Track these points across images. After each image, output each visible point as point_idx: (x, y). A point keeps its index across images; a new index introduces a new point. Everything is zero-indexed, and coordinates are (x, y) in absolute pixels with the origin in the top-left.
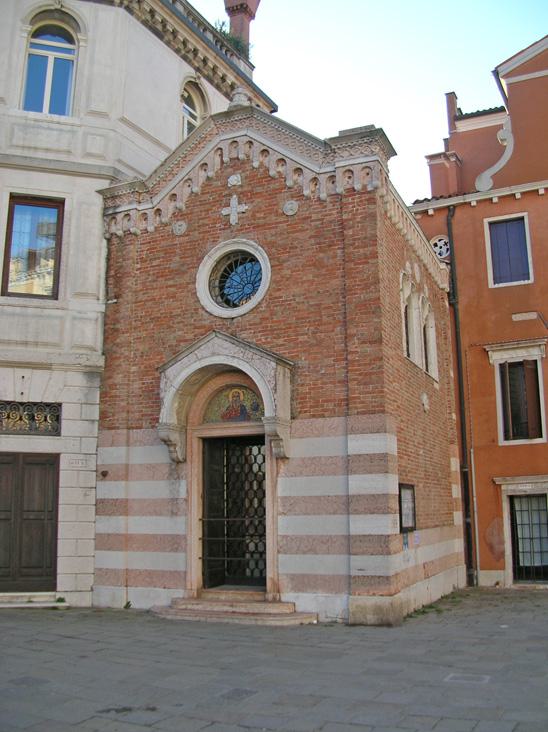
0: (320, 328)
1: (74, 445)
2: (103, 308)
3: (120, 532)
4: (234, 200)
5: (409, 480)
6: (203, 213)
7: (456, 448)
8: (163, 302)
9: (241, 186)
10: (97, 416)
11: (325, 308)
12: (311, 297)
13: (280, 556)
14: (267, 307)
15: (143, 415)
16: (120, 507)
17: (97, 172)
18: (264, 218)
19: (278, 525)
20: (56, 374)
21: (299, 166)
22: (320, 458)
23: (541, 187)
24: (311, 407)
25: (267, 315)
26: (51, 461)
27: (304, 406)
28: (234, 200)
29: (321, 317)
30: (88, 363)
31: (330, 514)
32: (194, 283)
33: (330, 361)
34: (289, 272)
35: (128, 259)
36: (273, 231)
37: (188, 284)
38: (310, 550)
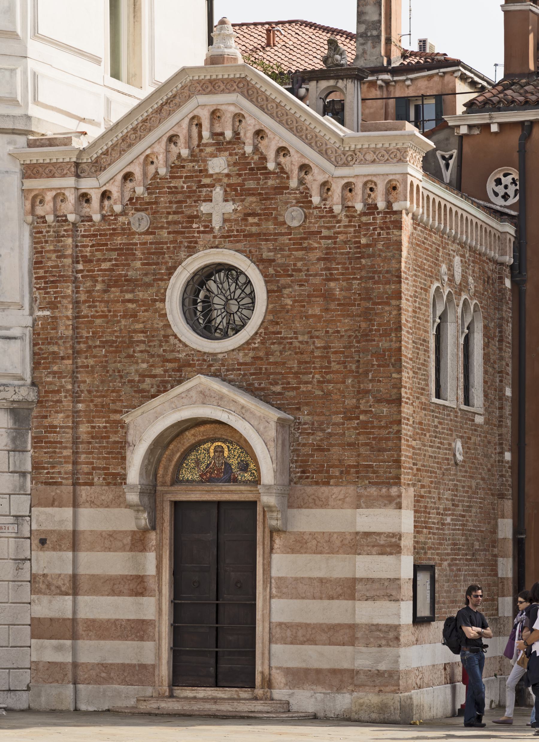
0: (328, 377)
2: (29, 321)
4: (218, 192)
5: (430, 559)
6: (175, 206)
7: (508, 505)
8: (119, 322)
9: (228, 175)
11: (335, 353)
12: (318, 337)
13: (274, 647)
14: (262, 343)
15: (94, 468)
18: (257, 225)
19: (274, 610)
25: (261, 354)
27: (306, 471)
28: (218, 192)
29: (329, 362)
30: (16, 398)
32: (163, 301)
33: (338, 419)
34: (289, 302)
36: (271, 245)
37: (155, 301)
38: (308, 640)
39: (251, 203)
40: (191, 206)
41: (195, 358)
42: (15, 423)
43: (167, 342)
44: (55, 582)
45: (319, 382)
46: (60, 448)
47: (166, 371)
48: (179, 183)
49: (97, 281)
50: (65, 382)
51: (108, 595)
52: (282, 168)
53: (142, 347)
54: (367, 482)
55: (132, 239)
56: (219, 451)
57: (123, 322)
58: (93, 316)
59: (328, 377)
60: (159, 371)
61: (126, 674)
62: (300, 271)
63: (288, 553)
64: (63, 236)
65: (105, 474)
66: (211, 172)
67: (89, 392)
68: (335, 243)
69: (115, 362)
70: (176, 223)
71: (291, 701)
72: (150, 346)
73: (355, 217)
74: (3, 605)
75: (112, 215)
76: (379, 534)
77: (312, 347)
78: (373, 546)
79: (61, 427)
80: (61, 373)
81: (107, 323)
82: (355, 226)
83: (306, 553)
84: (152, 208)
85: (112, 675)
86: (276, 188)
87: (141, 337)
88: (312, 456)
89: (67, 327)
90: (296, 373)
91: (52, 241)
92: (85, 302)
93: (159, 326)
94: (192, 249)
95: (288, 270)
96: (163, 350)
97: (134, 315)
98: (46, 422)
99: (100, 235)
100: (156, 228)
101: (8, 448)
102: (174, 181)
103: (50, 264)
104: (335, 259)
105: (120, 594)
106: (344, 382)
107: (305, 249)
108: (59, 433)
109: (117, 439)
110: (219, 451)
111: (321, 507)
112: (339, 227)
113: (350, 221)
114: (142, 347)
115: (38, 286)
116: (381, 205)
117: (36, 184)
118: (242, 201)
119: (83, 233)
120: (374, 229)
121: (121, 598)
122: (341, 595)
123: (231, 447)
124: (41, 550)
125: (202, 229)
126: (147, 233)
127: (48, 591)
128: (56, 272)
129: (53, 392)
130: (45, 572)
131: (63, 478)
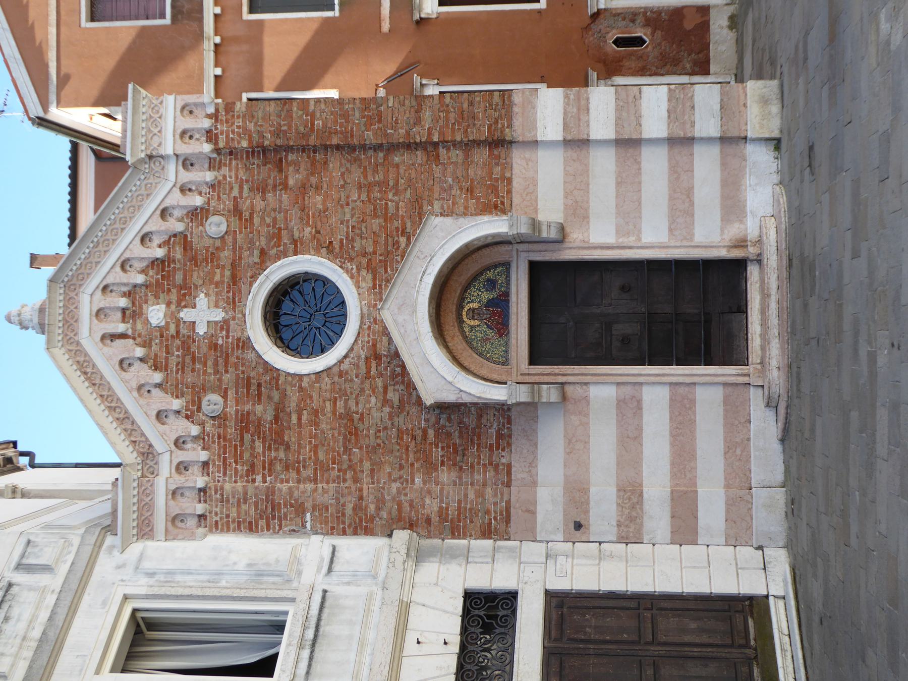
0: (391, 183)
1: (531, 573)
3: (662, 497)
4: (186, 315)
8: (323, 432)
9: (168, 304)
10: (488, 543)
11: (366, 177)
14: (351, 260)
16: (631, 496)
17: (90, 548)
20: (418, 596)
21: (158, 212)
22: (565, 182)
23: (210, 9)
24: (497, 196)
25: (364, 261)
26: (562, 607)
28: (186, 315)
30: (404, 551)
31: (640, 169)
34: (308, 230)
35: (245, 493)
36: (246, 254)
37: (300, 387)
38: (688, 197)
39: (199, 276)
40: (199, 347)
41: (366, 339)
42: (435, 556)
43: (347, 373)
44: (627, 511)
45: (395, 194)
46: (466, 504)
47: (381, 375)
48: (173, 361)
49: (276, 458)
50: (389, 495)
51: (641, 445)
52: (164, 242)
53: (352, 403)
54: (507, 130)
55: (231, 415)
56: (473, 313)
57: (323, 426)
58: (315, 464)
59: (391, 183)
60: (380, 382)
61: (737, 422)
62: (275, 220)
63: (588, 222)
64: (222, 495)
65: (498, 449)
66: (163, 324)
67: (401, 467)
68: (247, 181)
69: (368, 436)
70: (216, 364)
71: (761, 214)
72: (351, 394)
73: (221, 160)
74: (656, 574)
75: (204, 439)
76: (565, 113)
77: (358, 203)
78: (579, 120)
79: (442, 501)
80: (378, 500)
81: (323, 445)
82: (230, 159)
83: (588, 202)
84: (198, 392)
85: (738, 440)
86: (185, 249)
87: (340, 404)
88: (478, 199)
89: (325, 491)
90: (386, 220)
91: (228, 509)
92: (298, 472)
93: (329, 382)
94: (245, 344)
95: (274, 233)
96: (356, 377)
97: (316, 413)
98: (435, 519)
99: (225, 453)
100: (220, 387)
101: (464, 563)
102: (170, 366)
103: (252, 512)
104: (264, 180)
105: (639, 429)
106: (397, 166)
107: (252, 214)
108: (448, 504)
109: (457, 433)
110: (473, 313)
111: (536, 185)
112: (231, 177)
113: (225, 165)
114: (352, 403)
115: (277, 528)
116: (207, 124)
117: (160, 521)
118: (196, 287)
119: (221, 475)
120: (233, 132)
121: (645, 427)
122: (636, 160)
123: (468, 300)
124: (588, 529)
125: (224, 333)
126: (225, 397)
127: (638, 520)
128: (262, 504)
129: (400, 509)
130: (615, 523)
131: (502, 499)
